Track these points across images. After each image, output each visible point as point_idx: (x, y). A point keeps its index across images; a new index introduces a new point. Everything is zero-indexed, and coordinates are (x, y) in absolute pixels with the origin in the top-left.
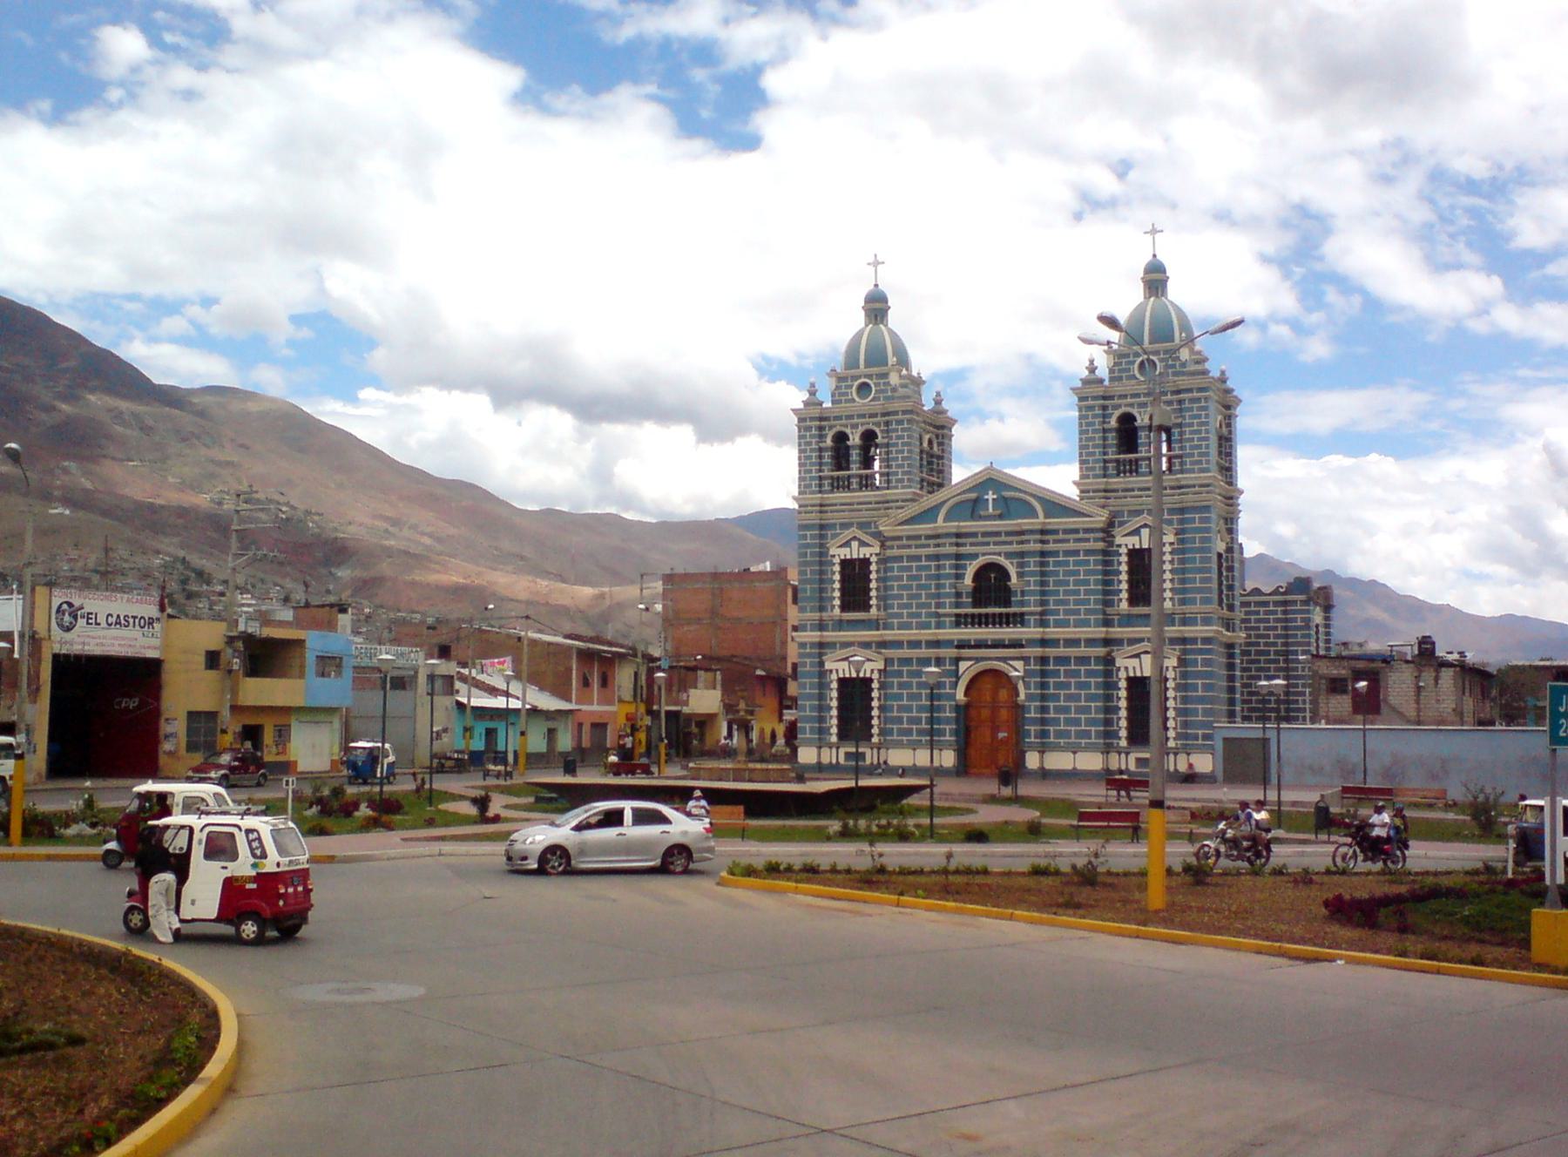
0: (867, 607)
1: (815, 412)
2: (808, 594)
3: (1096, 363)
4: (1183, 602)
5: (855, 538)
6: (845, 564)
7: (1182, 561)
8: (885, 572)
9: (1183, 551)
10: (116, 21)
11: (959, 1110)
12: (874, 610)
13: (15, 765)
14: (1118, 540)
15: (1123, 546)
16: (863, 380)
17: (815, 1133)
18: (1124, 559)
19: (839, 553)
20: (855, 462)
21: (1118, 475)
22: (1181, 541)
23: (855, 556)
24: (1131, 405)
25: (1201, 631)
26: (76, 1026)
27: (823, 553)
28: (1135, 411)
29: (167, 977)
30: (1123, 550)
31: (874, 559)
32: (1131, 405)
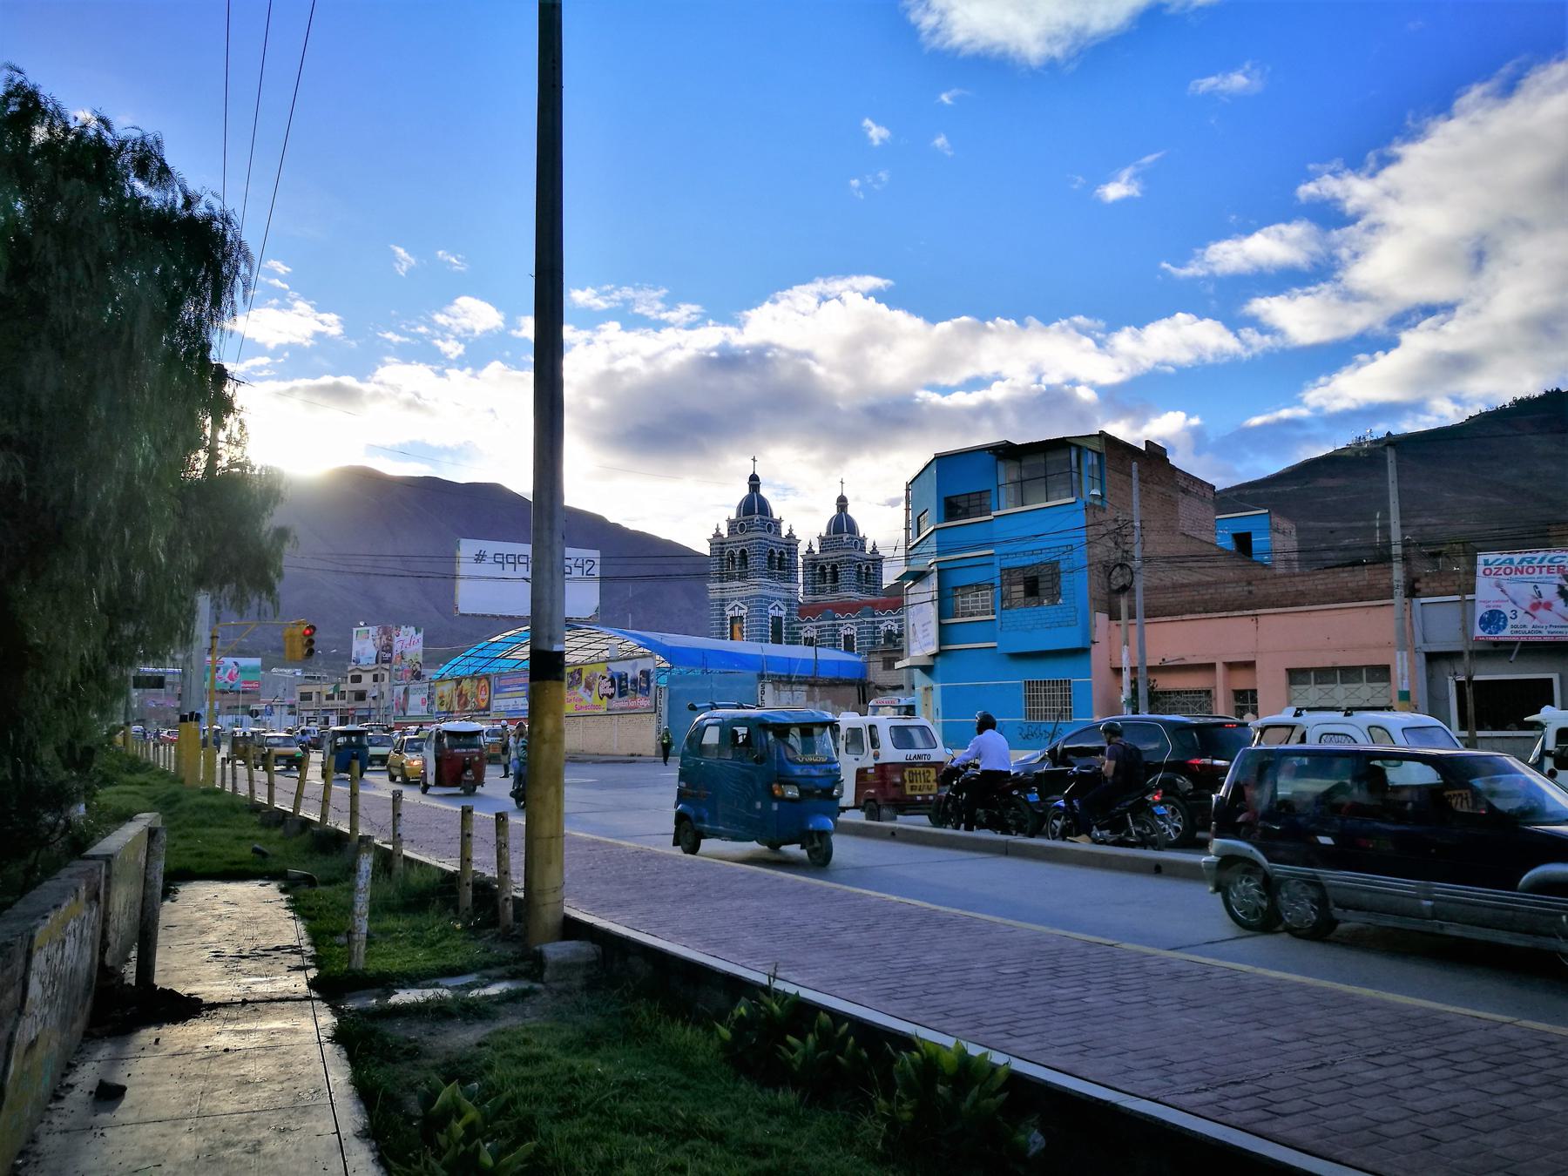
1: (719, 540)
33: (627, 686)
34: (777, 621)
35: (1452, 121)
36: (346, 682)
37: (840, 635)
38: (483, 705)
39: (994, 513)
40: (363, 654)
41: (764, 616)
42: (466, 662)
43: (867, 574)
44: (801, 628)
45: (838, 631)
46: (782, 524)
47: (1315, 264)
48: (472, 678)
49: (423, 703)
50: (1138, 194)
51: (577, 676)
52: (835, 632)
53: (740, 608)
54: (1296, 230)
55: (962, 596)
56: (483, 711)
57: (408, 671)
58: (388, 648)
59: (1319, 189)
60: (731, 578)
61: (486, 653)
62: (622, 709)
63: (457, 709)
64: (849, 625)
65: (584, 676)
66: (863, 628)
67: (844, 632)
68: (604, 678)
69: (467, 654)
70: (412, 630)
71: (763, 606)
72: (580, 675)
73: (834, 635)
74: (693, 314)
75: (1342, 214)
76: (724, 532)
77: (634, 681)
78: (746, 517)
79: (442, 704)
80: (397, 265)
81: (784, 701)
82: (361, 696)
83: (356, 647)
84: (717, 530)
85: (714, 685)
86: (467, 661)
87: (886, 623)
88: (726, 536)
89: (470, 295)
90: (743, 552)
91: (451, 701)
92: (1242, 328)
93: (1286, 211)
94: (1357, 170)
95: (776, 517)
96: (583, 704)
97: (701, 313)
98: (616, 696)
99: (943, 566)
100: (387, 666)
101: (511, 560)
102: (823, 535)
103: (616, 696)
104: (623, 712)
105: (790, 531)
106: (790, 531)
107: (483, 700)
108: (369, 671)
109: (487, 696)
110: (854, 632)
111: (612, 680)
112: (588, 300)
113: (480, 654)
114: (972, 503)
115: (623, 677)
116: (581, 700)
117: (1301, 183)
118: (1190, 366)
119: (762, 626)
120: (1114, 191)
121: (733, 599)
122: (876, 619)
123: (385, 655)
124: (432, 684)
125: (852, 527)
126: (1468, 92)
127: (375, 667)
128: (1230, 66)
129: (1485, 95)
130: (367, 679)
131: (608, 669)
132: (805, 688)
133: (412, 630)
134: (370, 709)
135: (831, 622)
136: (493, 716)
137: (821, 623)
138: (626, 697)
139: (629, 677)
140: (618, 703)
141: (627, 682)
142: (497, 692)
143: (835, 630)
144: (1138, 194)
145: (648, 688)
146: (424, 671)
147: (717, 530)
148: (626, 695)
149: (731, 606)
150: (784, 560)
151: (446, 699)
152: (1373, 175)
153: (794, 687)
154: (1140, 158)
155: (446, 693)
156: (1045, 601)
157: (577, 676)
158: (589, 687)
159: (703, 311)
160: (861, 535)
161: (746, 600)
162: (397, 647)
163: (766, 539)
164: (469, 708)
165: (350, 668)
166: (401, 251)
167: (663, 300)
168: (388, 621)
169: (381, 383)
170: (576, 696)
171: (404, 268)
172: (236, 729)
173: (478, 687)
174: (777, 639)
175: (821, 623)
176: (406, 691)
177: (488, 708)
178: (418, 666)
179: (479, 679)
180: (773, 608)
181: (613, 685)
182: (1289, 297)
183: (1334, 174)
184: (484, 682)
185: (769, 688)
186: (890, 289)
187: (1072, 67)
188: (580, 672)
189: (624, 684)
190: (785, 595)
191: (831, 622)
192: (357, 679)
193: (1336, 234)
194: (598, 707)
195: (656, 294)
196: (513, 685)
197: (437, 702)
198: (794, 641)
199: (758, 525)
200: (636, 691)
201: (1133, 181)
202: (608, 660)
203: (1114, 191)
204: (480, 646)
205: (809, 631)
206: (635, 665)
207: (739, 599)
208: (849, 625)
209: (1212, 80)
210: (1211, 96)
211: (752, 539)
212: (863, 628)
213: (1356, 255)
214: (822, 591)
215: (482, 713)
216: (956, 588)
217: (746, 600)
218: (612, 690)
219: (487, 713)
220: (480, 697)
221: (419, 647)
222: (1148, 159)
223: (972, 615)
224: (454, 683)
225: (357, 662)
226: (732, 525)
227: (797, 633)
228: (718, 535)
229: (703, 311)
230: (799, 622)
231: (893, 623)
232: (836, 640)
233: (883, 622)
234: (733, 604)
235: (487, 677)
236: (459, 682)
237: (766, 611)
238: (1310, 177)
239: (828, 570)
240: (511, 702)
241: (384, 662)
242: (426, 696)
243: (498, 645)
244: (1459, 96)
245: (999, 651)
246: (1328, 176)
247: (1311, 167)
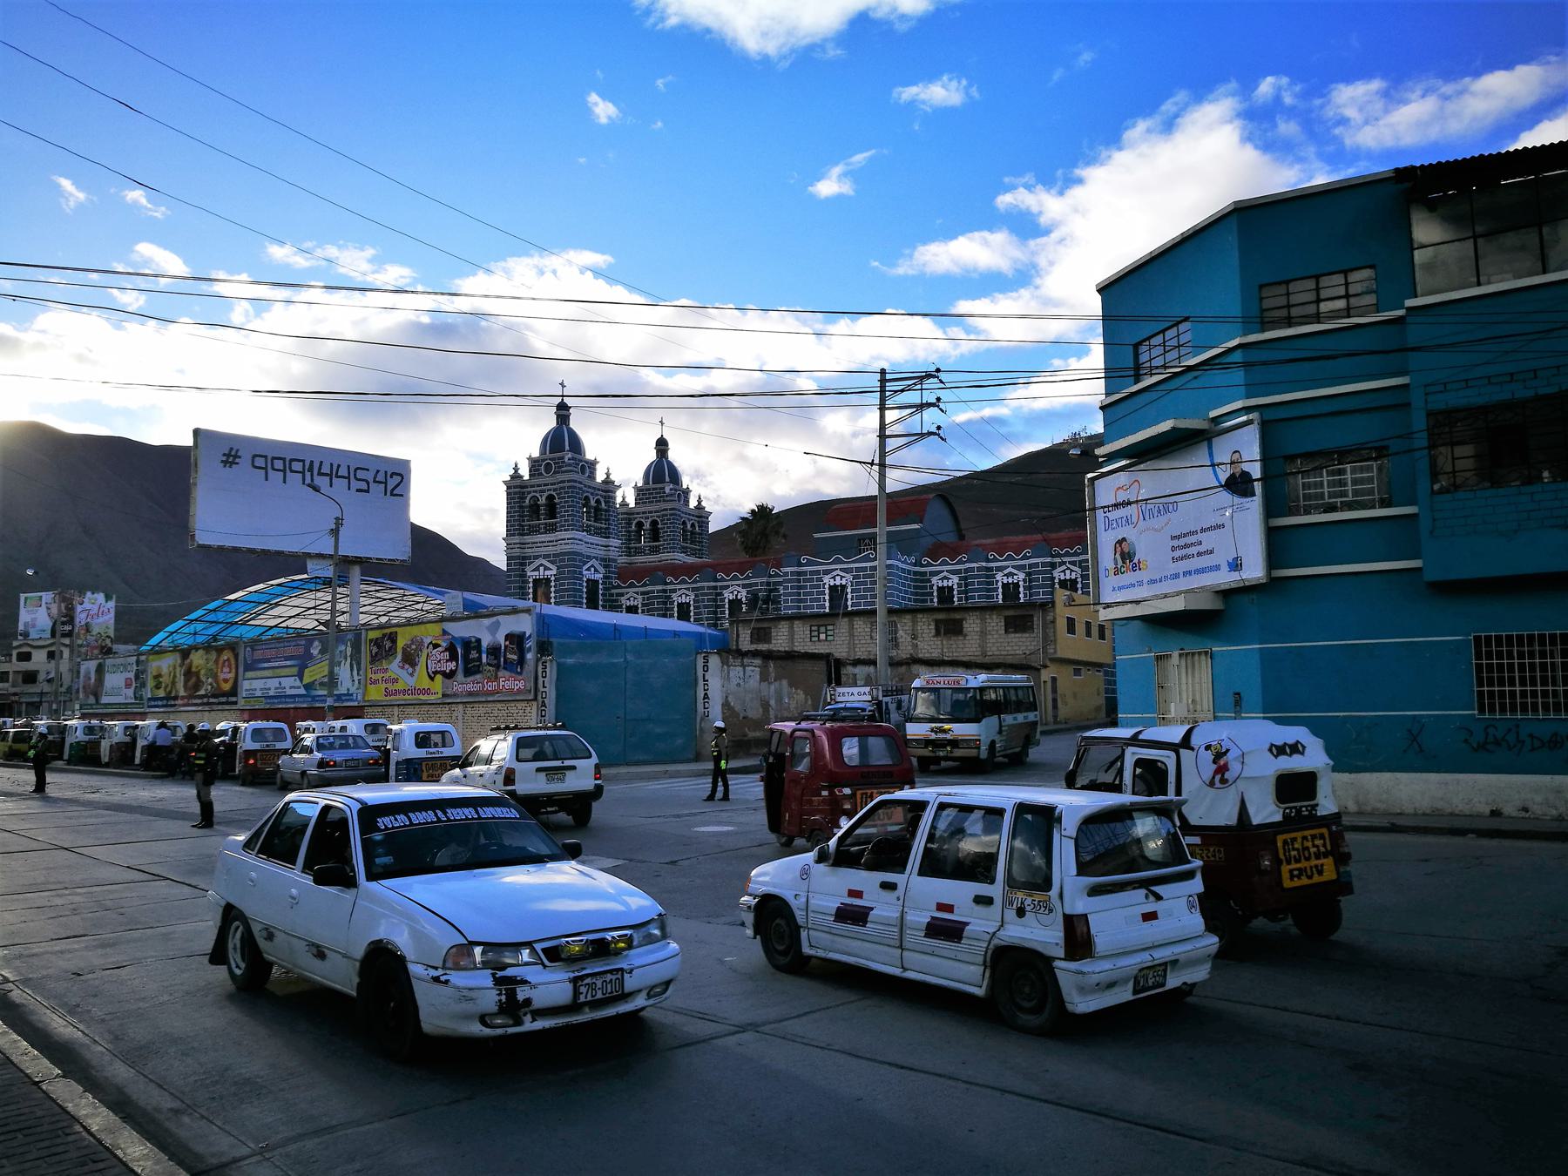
1: (518, 482)
2: (827, 610)
3: (519, 466)
6: (833, 588)
8: (967, 599)
9: (989, 590)
10: (998, 209)
11: (1098, 910)
13: (1139, 819)
14: (529, 574)
17: (764, 1024)
19: (532, 574)
20: (542, 514)
22: (1030, 581)
23: (1068, 578)
24: (536, 492)
27: (523, 575)
30: (531, 580)
31: (553, 578)
32: (536, 492)
33: (480, 658)
34: (593, 584)
35: (1122, 152)
36: (10, 661)
37: (672, 603)
38: (227, 687)
39: (1409, 303)
40: (34, 626)
41: (577, 579)
42: (191, 628)
43: (692, 533)
44: (622, 595)
45: (670, 597)
46: (598, 466)
47: (1017, 270)
48: (207, 648)
49: (128, 685)
50: (851, 193)
51: (388, 644)
52: (666, 598)
53: (546, 568)
54: (1000, 238)
55: (1305, 473)
56: (225, 698)
57: (96, 648)
58: (70, 617)
59: (1015, 199)
60: (534, 530)
61: (221, 616)
62: (470, 694)
63: (182, 693)
64: (838, 572)
65: (401, 643)
66: (703, 594)
67: (677, 599)
68: (436, 646)
69: (193, 616)
70: (101, 597)
71: (575, 566)
72: (394, 641)
73: (665, 603)
74: (402, 277)
75: (1038, 225)
76: (525, 472)
77: (494, 651)
78: (552, 455)
79: (158, 687)
80: (62, 200)
81: (735, 681)
82: (30, 677)
83: (24, 617)
84: (516, 469)
85: (630, 657)
86: (192, 626)
87: (731, 589)
88: (526, 477)
89: (151, 241)
90: (551, 498)
91: (174, 683)
92: (949, 327)
93: (989, 220)
94: (1047, 187)
95: (589, 456)
96: (399, 686)
97: (410, 277)
98: (460, 676)
99: (1271, 415)
100: (67, 641)
101: (279, 464)
102: (640, 484)
103: (460, 676)
104: (473, 699)
105: (608, 475)
106: (608, 475)
107: (226, 681)
108: (43, 647)
109: (232, 675)
110: (690, 599)
111: (451, 649)
112: (288, 257)
113: (212, 617)
114: (1294, 299)
115: (471, 645)
116: (396, 681)
117: (999, 194)
118: (902, 361)
119: (575, 590)
120: (827, 188)
121: (537, 557)
122: (719, 584)
123: (65, 625)
124: (143, 658)
125: (675, 476)
126: (1134, 126)
127: (52, 641)
128: (931, 76)
129: (1149, 131)
130: (39, 657)
131: (445, 632)
132: (758, 662)
133: (101, 597)
134: (42, 694)
135: (660, 587)
136: (241, 704)
137: (699, 585)
138: (478, 677)
139: (484, 644)
140: (462, 684)
141: (480, 652)
142: (248, 668)
143: (718, 594)
144: (851, 193)
145: (522, 661)
146: (115, 647)
147: (516, 469)
148: (478, 672)
149: (533, 566)
150: (601, 510)
151: (165, 680)
152: (1061, 193)
153: (746, 661)
154: (851, 156)
155: (165, 671)
156: (1546, 474)
157: (388, 644)
158: (410, 660)
159: (415, 275)
160: (685, 487)
161: (554, 558)
162: (80, 618)
163: (580, 483)
164: (202, 692)
165: (15, 644)
166: (66, 184)
167: (370, 261)
168: (67, 588)
169: (43, 332)
170: (387, 676)
171: (72, 204)
172: (1057, 581)
173: (216, 662)
174: (592, 604)
175: (699, 585)
176: (100, 670)
177: (234, 692)
178: (108, 641)
179: (220, 650)
180: (588, 569)
181: (453, 657)
182: (992, 301)
183: (1029, 188)
184: (226, 655)
185: (714, 661)
186: (610, 266)
187: (786, 64)
188: (393, 638)
189: (474, 654)
190: (601, 553)
191: (660, 587)
192: (25, 657)
193: (1032, 243)
194: (427, 692)
195: (363, 254)
196: (276, 658)
197: (151, 683)
198: (613, 606)
199: (570, 465)
200: (498, 667)
201: (843, 179)
202: (442, 620)
203: (827, 188)
204: (212, 606)
205: (632, 596)
206: (494, 629)
207: (545, 557)
208: (838, 572)
209: (913, 90)
210: (912, 104)
211: (563, 482)
212: (703, 594)
213: (1051, 263)
214: (639, 552)
215: (223, 699)
216: (1291, 458)
217: (554, 558)
218: (452, 665)
219: (234, 699)
220: (222, 676)
221: (110, 618)
222: (859, 158)
223: (1331, 508)
224: (177, 658)
225: (26, 635)
226: (534, 463)
227: (616, 601)
228: (516, 476)
229: (415, 275)
230: (619, 587)
231: (740, 589)
232: (717, 606)
233: (674, 591)
234: (537, 563)
235: (232, 647)
236: (185, 654)
237: (581, 573)
238: (1010, 188)
239: (647, 526)
240: (273, 683)
241: (64, 635)
242: (131, 675)
243: (237, 605)
244: (1127, 128)
245: (1430, 576)
246: (1022, 189)
247: (1006, 180)
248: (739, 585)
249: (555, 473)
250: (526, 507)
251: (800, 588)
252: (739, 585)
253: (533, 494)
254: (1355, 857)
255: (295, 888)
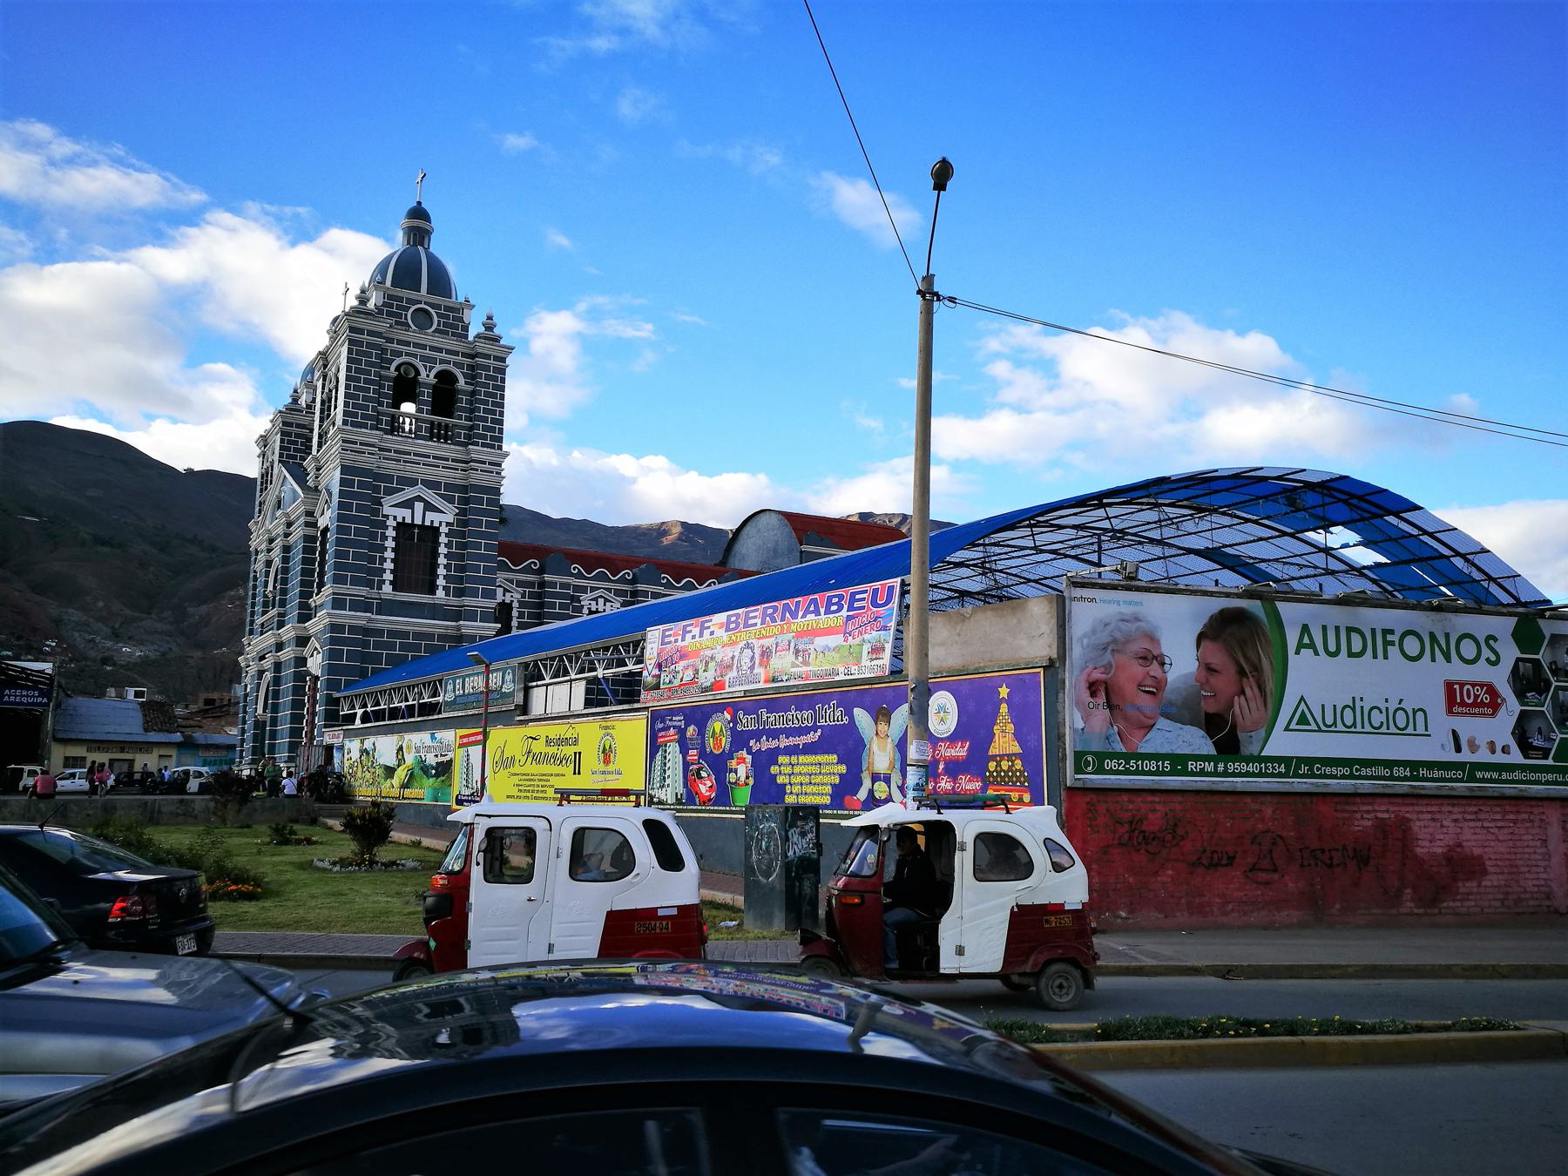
0: (432, 589)
4: (460, 593)
5: (419, 498)
7: (373, 536)
12: (440, 593)
14: (387, 510)
15: (391, 518)
16: (423, 306)
18: (391, 533)
19: (393, 512)
21: (431, 439)
22: (464, 523)
23: (418, 521)
24: (415, 356)
25: (351, 617)
26: (1126, 799)
28: (419, 365)
29: (1431, 559)
30: (391, 523)
31: (444, 529)
32: (415, 356)
121: (412, 482)
190: (455, 476)
234: (409, 493)
248: (609, 590)
249: (436, 331)
250: (387, 378)
251: (365, 658)
252: (609, 590)
253: (404, 359)
254: (1102, 954)
255: (414, 953)
